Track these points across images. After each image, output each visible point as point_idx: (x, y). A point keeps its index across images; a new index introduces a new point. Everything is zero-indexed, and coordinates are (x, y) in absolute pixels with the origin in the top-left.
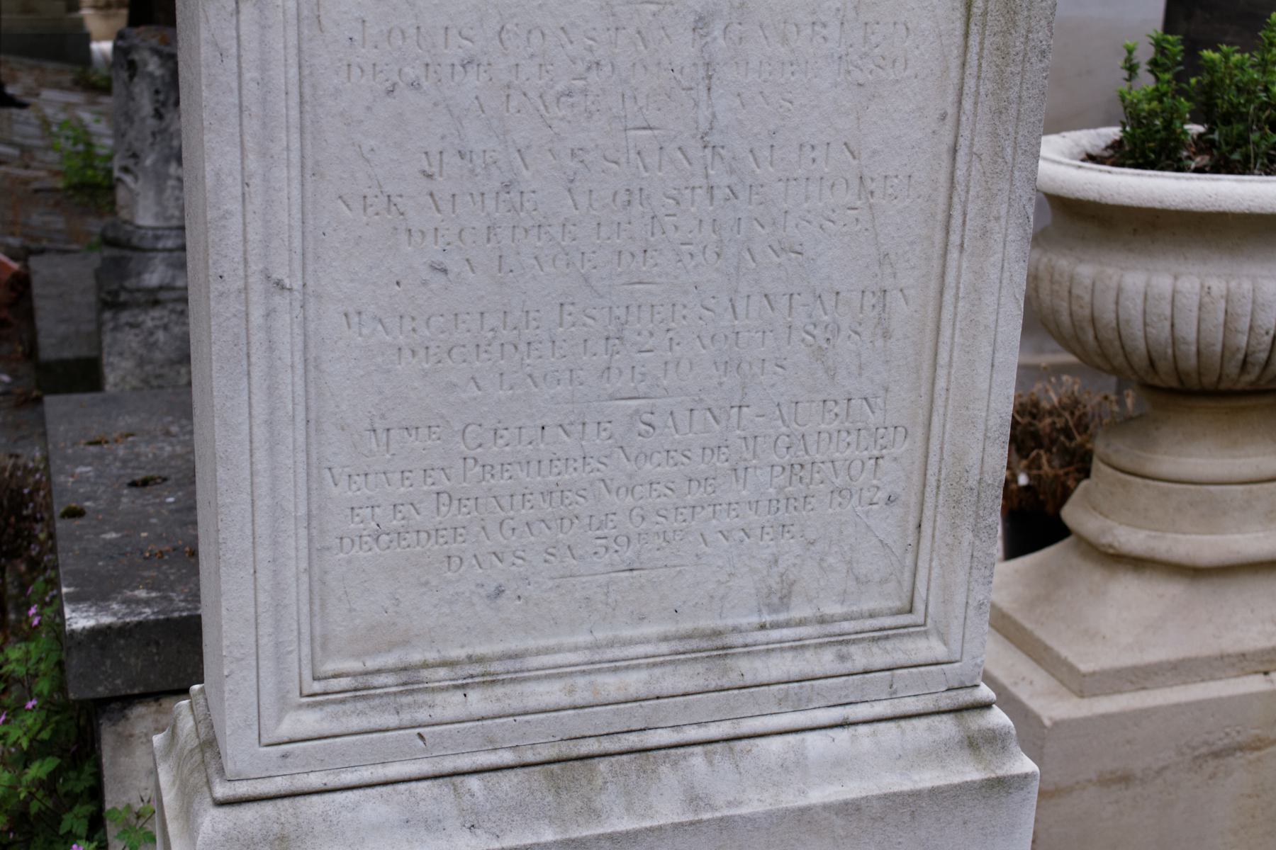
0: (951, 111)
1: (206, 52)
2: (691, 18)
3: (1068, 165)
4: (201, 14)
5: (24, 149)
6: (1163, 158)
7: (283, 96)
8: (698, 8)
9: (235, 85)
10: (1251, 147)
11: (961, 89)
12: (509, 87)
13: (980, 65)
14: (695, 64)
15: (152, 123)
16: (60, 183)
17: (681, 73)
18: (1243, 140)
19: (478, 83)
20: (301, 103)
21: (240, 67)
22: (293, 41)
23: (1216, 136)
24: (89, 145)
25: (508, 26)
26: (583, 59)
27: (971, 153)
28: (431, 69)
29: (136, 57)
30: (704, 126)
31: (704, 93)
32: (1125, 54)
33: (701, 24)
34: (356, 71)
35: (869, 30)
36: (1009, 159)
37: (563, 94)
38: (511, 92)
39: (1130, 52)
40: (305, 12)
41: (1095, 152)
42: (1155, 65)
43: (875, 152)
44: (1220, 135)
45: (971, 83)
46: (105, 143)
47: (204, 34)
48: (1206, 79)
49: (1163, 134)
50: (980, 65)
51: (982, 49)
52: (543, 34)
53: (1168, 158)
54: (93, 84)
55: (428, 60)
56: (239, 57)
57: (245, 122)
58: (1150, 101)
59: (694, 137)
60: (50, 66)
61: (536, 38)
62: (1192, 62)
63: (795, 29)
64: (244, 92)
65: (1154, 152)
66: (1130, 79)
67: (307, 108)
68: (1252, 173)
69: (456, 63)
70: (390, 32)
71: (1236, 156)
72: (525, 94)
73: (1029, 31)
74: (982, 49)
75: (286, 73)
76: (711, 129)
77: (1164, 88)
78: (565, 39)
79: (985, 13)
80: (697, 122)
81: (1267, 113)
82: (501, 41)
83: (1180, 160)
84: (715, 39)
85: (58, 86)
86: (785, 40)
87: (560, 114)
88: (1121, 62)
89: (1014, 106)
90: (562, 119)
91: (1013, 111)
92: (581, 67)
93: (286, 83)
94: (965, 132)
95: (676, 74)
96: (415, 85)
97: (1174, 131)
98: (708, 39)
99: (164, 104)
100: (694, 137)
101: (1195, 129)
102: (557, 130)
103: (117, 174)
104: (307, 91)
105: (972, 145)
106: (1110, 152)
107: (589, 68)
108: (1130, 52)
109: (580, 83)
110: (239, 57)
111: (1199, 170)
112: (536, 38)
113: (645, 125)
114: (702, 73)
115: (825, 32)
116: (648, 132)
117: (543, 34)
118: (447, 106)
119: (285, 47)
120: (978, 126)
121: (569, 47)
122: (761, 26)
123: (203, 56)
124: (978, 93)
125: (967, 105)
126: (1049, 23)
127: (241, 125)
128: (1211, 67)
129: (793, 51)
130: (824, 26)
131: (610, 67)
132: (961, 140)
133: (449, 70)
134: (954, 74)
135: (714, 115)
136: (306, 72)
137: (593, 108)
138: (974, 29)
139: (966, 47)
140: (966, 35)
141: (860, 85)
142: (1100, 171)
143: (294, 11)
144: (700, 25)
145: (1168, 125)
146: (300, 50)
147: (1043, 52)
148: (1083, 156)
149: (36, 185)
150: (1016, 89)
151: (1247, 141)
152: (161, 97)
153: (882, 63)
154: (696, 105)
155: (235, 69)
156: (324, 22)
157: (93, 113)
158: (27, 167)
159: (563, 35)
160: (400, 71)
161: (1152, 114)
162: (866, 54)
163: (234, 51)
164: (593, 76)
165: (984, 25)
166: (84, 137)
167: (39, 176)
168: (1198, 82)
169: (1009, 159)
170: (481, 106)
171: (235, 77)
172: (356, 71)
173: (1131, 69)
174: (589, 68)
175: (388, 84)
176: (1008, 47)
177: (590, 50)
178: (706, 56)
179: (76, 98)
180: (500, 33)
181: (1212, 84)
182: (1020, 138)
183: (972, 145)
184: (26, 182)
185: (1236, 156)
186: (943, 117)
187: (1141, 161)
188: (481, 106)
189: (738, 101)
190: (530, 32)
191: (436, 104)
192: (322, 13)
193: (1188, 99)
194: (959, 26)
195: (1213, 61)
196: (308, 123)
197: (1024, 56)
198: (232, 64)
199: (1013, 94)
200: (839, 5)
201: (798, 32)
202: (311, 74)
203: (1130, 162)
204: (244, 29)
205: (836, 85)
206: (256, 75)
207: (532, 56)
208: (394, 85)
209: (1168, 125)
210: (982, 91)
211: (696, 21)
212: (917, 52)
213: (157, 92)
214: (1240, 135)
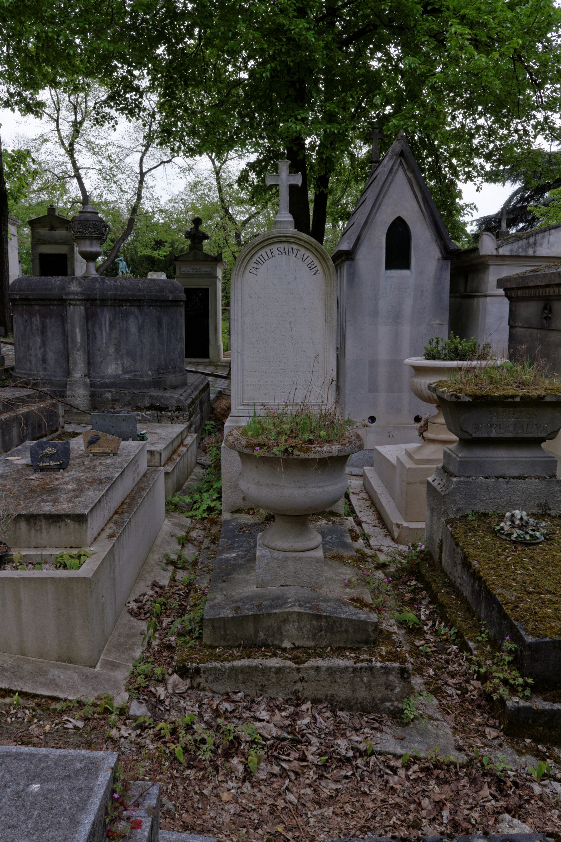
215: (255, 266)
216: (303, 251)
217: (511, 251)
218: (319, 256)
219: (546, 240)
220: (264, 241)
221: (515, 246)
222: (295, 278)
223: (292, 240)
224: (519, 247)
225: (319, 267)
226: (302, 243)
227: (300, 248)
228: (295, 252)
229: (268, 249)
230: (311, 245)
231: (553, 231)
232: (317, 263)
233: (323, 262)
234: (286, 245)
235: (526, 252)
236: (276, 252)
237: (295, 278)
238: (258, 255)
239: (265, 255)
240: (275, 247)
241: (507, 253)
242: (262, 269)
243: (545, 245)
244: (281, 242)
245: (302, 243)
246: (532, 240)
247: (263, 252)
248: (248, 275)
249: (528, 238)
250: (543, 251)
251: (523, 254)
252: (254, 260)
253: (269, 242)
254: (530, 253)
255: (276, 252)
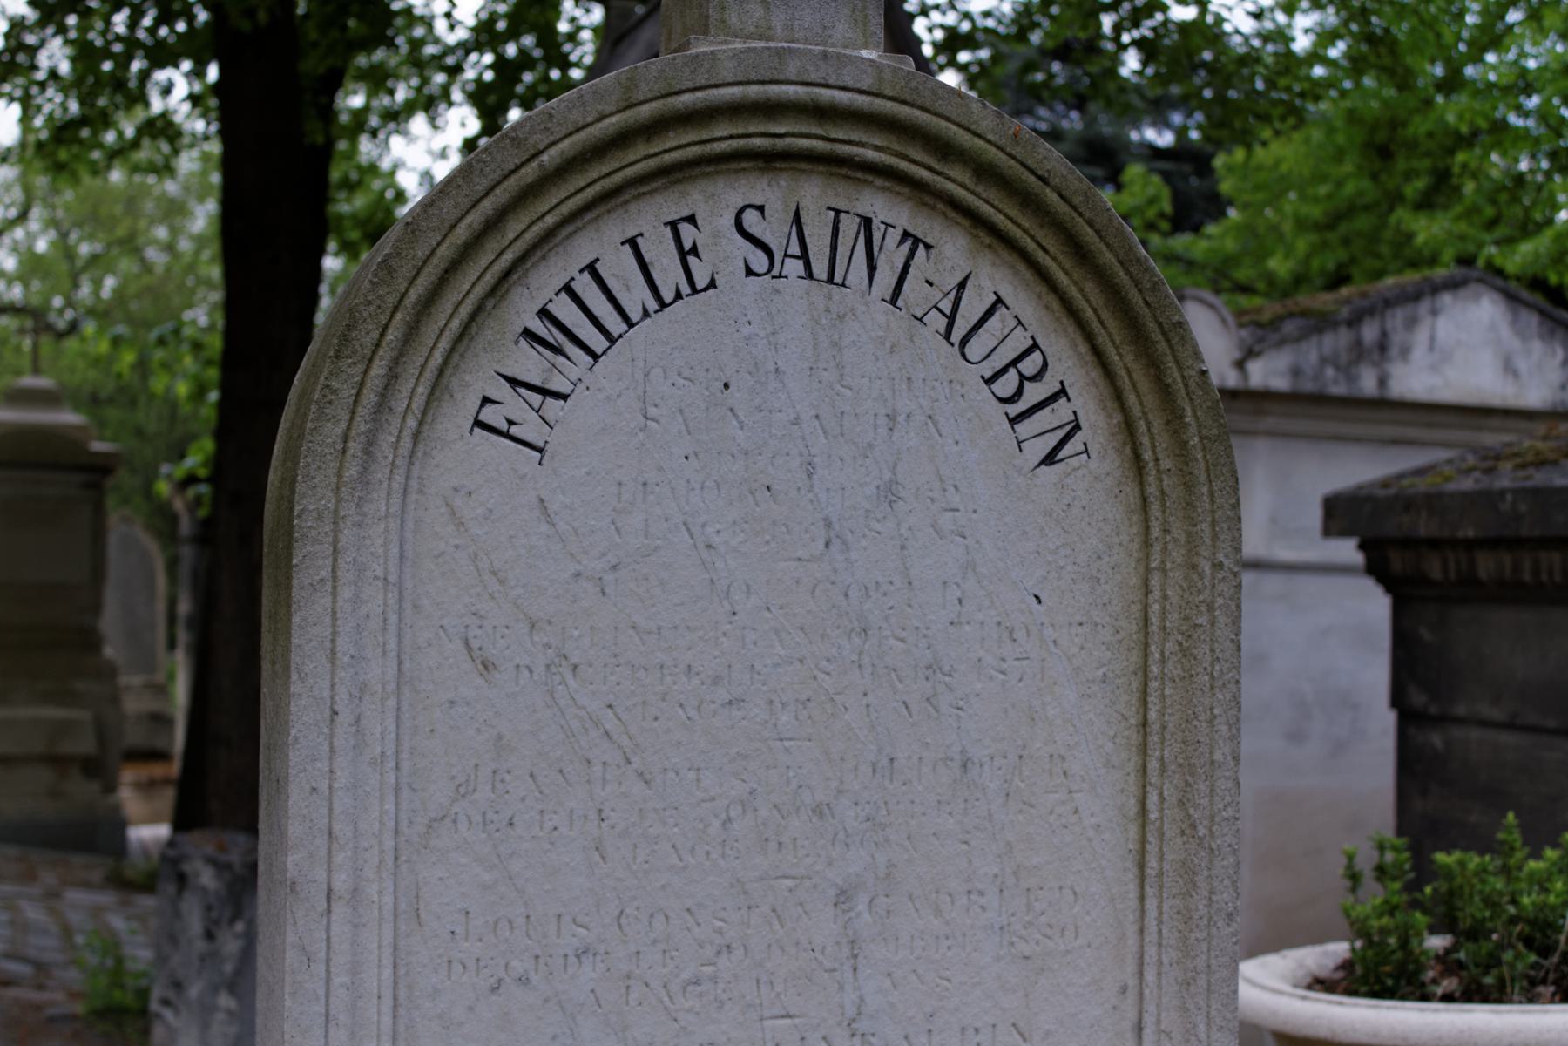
0: (1132, 982)
1: (291, 957)
2: (832, 892)
3: (1291, 995)
4: (289, 916)
5: (40, 967)
6: (1403, 982)
7: (375, 1001)
8: (839, 881)
9: (321, 992)
10: (1505, 969)
11: (1141, 957)
12: (628, 977)
13: (1160, 931)
14: (838, 943)
15: (200, 945)
16: (80, 1008)
17: (823, 953)
18: (1492, 962)
19: (594, 975)
20: (395, 1007)
21: (328, 971)
22: (388, 939)
23: (1462, 955)
24: (119, 961)
25: (628, 911)
26: (711, 943)
27: (1160, 1031)
28: (541, 961)
29: (186, 868)
30: (851, 1011)
31: (849, 975)
32: (1344, 861)
33: (843, 897)
34: (457, 968)
35: (1032, 897)
36: (1203, 1036)
37: (690, 983)
38: (632, 982)
39: (1351, 858)
40: (403, 906)
41: (1323, 973)
42: (1381, 871)
43: (1048, 1033)
44: (1467, 954)
45: (1151, 952)
46: (140, 955)
47: (291, 938)
48: (1444, 887)
49: (1399, 955)
50: (1160, 931)
51: (1161, 913)
52: (667, 917)
53: (1409, 983)
54: (130, 881)
55: (538, 952)
56: (328, 961)
57: (332, 1032)
58: (1381, 915)
59: (839, 1024)
60: (78, 860)
61: (659, 922)
62: (1423, 870)
63: (948, 899)
64: (332, 999)
65: (1390, 975)
66: (1353, 890)
67: (401, 1011)
68: (1510, 1002)
69: (570, 953)
70: (496, 923)
71: (1489, 980)
72: (647, 985)
73: (1212, 892)
74: (1161, 913)
75: (380, 974)
76: (859, 1014)
77: (1395, 899)
78: (691, 922)
79: (1160, 874)
80: (842, 1007)
81: (1519, 928)
82: (620, 926)
83: (1423, 985)
84: (859, 914)
85: (86, 885)
86: (938, 912)
87: (687, 1005)
88: (1341, 871)
89: (1203, 976)
90: (690, 1010)
91: (1202, 981)
92: (709, 952)
93: (379, 987)
94: (1150, 1007)
95: (817, 954)
96: (523, 981)
97: (1411, 952)
98: (852, 914)
99: (217, 923)
100: (839, 1024)
101: (1437, 942)
102: (683, 1023)
103: (154, 1006)
104: (403, 993)
105: (1159, 1022)
106: (1340, 974)
107: (719, 952)
108: (1351, 858)
109: (708, 970)
110: (328, 961)
111: (1448, 998)
112: (659, 922)
113: (784, 1013)
114: (846, 951)
115: (982, 901)
116: (787, 1021)
117: (667, 917)
118: (559, 1002)
119: (380, 947)
120: (1164, 1000)
121: (696, 930)
122: (910, 897)
123: (288, 961)
124: (1160, 963)
125: (1150, 976)
126: (1234, 883)
127: (326, 1036)
128: (1448, 874)
129: (947, 923)
130: (981, 894)
131: (742, 950)
132: (1146, 1016)
133: (561, 961)
134: (1132, 940)
135: (862, 999)
136: (402, 971)
137: (724, 997)
138: (1149, 891)
139: (1143, 911)
140: (1142, 898)
141: (1026, 958)
142: (1330, 1002)
143: (390, 906)
144: (842, 899)
145: (1404, 943)
146: (395, 948)
147: (1230, 915)
148: (1309, 980)
149: (52, 1011)
150: (1204, 957)
151: (1499, 963)
152: (214, 914)
153: (1049, 932)
154: (841, 988)
155: (323, 975)
156: (423, 915)
157: (128, 918)
158: (41, 987)
159: (688, 917)
160: (507, 965)
161: (1384, 931)
162: (1030, 923)
163: (323, 954)
164: (723, 961)
165: (1161, 887)
166: (112, 946)
167: (56, 1000)
168: (1435, 890)
169: (1203, 1036)
170: (597, 1000)
171: (322, 983)
172: (457, 968)
173: (1354, 877)
174: (719, 952)
175: (492, 980)
176: (1189, 910)
177: (720, 932)
178: (850, 933)
179: (106, 898)
180: (619, 918)
181: (1451, 893)
182: (1213, 1013)
183: (1159, 1022)
184: (39, 1007)
185: (1489, 980)
186: (1124, 990)
187: (1377, 988)
188: (597, 1000)
189: (888, 983)
190: (652, 915)
191: (546, 1001)
192: (422, 906)
193: (1425, 912)
194: (1133, 888)
195: (1447, 867)
196: (401, 1029)
197: (1210, 920)
198: (320, 969)
199: (1201, 962)
200: (996, 870)
201: (953, 902)
202: (407, 974)
203: (1364, 989)
204: (335, 930)
205: (998, 959)
206: (345, 979)
207: (655, 941)
208: (500, 981)
209: (1404, 943)
210: (1165, 960)
211: (837, 895)
212: (1088, 919)
213: (209, 908)
214: (1491, 955)
215: (530, 364)
216: (953, 251)
217: (1296, 372)
218: (1089, 297)
219: (1421, 336)
220: (622, 139)
221: (1310, 353)
222: (889, 493)
223: (870, 148)
224: (1324, 360)
225: (1086, 402)
226: (956, 182)
227: (926, 226)
228: (891, 256)
229: (648, 219)
230: (1029, 201)
231: (1446, 298)
232: (1066, 362)
233: (1123, 359)
234: (814, 195)
235: (1352, 379)
236: (723, 251)
237: (889, 493)
238: (564, 265)
239: (620, 269)
240: (714, 205)
241: (1280, 383)
242: (601, 393)
243: (1419, 353)
244: (770, 160)
245: (956, 182)
246: (1369, 332)
247: (603, 242)
248: (461, 459)
249: (1354, 322)
250: (1415, 379)
251: (1339, 389)
252: (522, 310)
253: (677, 146)
254: (1368, 383)
255: (723, 251)
